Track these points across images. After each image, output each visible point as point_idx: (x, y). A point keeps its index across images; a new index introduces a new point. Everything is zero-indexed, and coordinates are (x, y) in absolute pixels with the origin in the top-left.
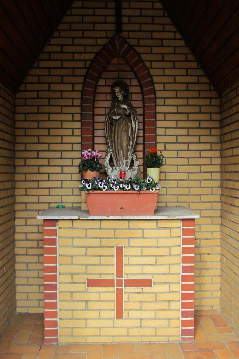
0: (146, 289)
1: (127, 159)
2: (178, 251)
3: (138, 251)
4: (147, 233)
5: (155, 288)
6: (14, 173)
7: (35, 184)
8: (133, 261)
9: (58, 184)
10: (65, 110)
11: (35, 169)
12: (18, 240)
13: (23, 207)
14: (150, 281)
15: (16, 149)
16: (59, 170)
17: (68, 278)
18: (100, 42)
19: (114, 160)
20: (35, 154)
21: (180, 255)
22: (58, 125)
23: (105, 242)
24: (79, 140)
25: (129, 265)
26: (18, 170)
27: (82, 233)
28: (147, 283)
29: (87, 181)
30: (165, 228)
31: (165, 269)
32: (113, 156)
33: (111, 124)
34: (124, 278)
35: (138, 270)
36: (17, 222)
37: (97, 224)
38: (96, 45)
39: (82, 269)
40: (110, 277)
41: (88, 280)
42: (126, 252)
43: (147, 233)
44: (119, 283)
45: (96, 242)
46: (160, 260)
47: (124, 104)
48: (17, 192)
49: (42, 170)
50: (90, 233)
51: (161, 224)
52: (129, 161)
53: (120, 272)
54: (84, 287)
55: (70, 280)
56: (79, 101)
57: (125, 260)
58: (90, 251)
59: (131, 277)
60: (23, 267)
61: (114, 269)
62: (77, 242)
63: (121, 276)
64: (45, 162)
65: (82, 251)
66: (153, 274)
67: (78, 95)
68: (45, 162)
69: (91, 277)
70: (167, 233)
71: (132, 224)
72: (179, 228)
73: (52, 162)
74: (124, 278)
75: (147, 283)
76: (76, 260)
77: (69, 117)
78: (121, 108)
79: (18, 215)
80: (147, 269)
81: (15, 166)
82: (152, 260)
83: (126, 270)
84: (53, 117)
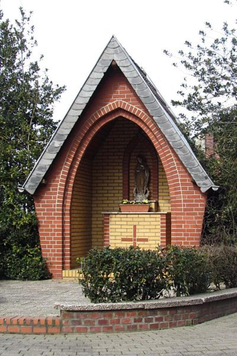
0: (146, 243)
1: (143, 190)
2: (159, 227)
3: (142, 227)
4: (146, 219)
5: (150, 242)
6: (92, 197)
7: (101, 202)
8: (140, 231)
9: (112, 202)
10: (116, 168)
11: (101, 195)
12: (93, 235)
13: (95, 212)
14: (147, 239)
15: (93, 192)
16: (112, 195)
17: (114, 238)
18: (131, 136)
19: (138, 191)
20: (101, 188)
21: (159, 229)
22: (112, 174)
23: (129, 223)
24: (121, 181)
25: (138, 232)
26: (94, 195)
27: (119, 219)
28: (146, 240)
29: (10, 144)
30: (153, 218)
31: (154, 234)
32: (137, 189)
33: (136, 174)
34: (137, 238)
35: (143, 234)
36: (93, 219)
37: (125, 216)
38: (130, 138)
39: (120, 234)
40: (131, 237)
41: (122, 238)
42: (137, 227)
43: (146, 219)
44: (135, 240)
45: (125, 223)
46: (152, 230)
47: (142, 165)
48: (93, 205)
49: (105, 195)
50: (123, 219)
51: (152, 216)
52: (145, 191)
53: (135, 236)
54: (120, 241)
55: (114, 238)
56: (122, 163)
57: (137, 231)
58: (123, 227)
59: (139, 238)
60: (96, 240)
61: (132, 234)
62: (117, 223)
63: (136, 237)
64: (106, 192)
65: (120, 227)
66: (148, 236)
67: (121, 161)
68: (106, 192)
69: (123, 237)
70: (154, 219)
71: (140, 216)
72: (159, 217)
73: (109, 192)
74: (137, 238)
75: (146, 240)
76: (117, 230)
77: (117, 171)
78: (140, 167)
79: (93, 216)
80: (146, 234)
81: (92, 194)
82: (148, 231)
83: (137, 234)
84: (110, 171)
